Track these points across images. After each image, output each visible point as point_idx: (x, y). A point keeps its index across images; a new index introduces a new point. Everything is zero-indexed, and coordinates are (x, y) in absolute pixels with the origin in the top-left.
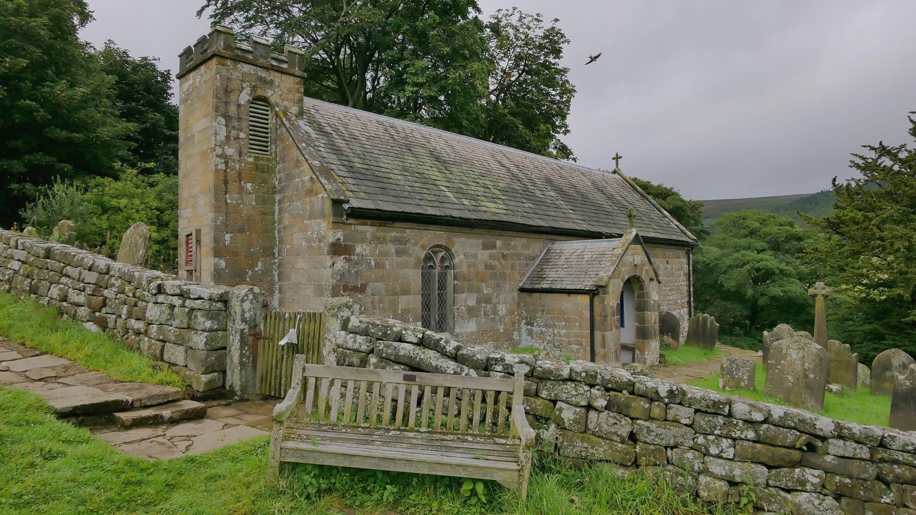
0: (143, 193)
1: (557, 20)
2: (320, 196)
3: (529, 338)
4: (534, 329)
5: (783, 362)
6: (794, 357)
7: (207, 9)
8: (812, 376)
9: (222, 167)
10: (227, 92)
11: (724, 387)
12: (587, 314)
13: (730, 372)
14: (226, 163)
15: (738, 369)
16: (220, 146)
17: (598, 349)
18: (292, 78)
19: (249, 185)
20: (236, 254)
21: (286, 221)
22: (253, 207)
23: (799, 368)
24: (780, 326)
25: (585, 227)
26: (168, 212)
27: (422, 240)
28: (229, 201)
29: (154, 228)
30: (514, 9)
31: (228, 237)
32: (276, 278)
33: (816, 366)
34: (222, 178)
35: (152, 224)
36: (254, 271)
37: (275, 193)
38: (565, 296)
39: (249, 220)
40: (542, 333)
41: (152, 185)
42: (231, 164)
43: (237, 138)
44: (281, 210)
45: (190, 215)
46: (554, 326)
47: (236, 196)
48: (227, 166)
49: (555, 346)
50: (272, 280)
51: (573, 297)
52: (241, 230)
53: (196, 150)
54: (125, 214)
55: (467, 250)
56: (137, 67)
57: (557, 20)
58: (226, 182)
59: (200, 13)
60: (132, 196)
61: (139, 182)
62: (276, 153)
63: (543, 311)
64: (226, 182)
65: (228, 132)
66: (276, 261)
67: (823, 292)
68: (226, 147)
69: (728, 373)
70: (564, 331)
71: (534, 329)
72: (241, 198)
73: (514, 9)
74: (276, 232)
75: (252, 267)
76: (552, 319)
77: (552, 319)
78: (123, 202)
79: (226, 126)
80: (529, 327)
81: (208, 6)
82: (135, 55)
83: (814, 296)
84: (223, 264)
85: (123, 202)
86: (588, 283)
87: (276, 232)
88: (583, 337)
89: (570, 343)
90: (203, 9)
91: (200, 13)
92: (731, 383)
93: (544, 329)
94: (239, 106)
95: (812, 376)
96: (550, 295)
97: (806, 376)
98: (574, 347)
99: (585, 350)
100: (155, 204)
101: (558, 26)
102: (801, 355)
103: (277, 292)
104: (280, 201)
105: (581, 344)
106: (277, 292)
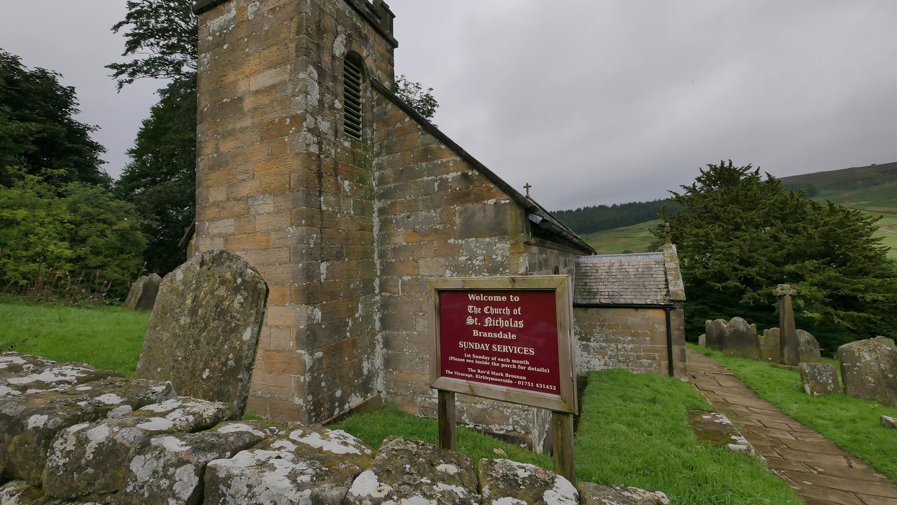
0: (50, 204)
1: (431, 89)
2: (491, 202)
3: (585, 354)
4: (590, 344)
5: (858, 364)
6: (868, 358)
7: (125, 26)
8: (891, 376)
9: (314, 149)
10: (320, 31)
11: (812, 393)
12: (663, 328)
13: (814, 378)
14: (319, 143)
15: (820, 374)
16: (312, 114)
17: (677, 363)
18: (384, 42)
19: (347, 183)
20: (333, 295)
21: (400, 238)
22: (351, 217)
23: (876, 369)
24: (735, 318)
26: (85, 226)
28: (324, 208)
29: (66, 244)
30: (402, 76)
31: (323, 267)
32: (378, 325)
33: (892, 366)
34: (314, 167)
35: (63, 239)
36: (355, 320)
37: (372, 198)
38: (632, 311)
39: (347, 239)
40: (601, 348)
41: (60, 195)
42: (325, 147)
43: (332, 107)
44: (384, 224)
45: (232, 230)
46: (617, 341)
47: (332, 199)
48: (320, 149)
49: (619, 361)
50: (373, 329)
51: (640, 312)
52: (339, 256)
53: (248, 122)
54: (23, 228)
56: (29, 78)
57: (431, 89)
58: (320, 176)
59: (116, 27)
60: (33, 207)
61: (43, 191)
62: (372, 139)
63: (602, 326)
64: (320, 176)
65: (322, 94)
66: (377, 298)
67: (790, 292)
68: (319, 119)
69: (812, 379)
70: (631, 346)
71: (590, 344)
72: (338, 204)
73: (402, 76)
74: (376, 256)
75: (352, 312)
76: (614, 334)
77: (614, 334)
78: (21, 214)
79: (319, 83)
80: (584, 342)
81: (128, 23)
82: (29, 65)
83: (781, 297)
84: (318, 314)
85: (21, 214)
86: (660, 298)
87: (376, 256)
88: (655, 350)
89: (639, 357)
90: (120, 24)
91: (116, 27)
92: (817, 388)
93: (604, 344)
94: (334, 57)
95: (891, 376)
96: (611, 311)
97: (886, 377)
98: (645, 361)
99: (659, 365)
100: (68, 217)
101: (431, 94)
102: (874, 356)
103: (379, 347)
104: (382, 211)
105: (654, 358)
106: (379, 347)
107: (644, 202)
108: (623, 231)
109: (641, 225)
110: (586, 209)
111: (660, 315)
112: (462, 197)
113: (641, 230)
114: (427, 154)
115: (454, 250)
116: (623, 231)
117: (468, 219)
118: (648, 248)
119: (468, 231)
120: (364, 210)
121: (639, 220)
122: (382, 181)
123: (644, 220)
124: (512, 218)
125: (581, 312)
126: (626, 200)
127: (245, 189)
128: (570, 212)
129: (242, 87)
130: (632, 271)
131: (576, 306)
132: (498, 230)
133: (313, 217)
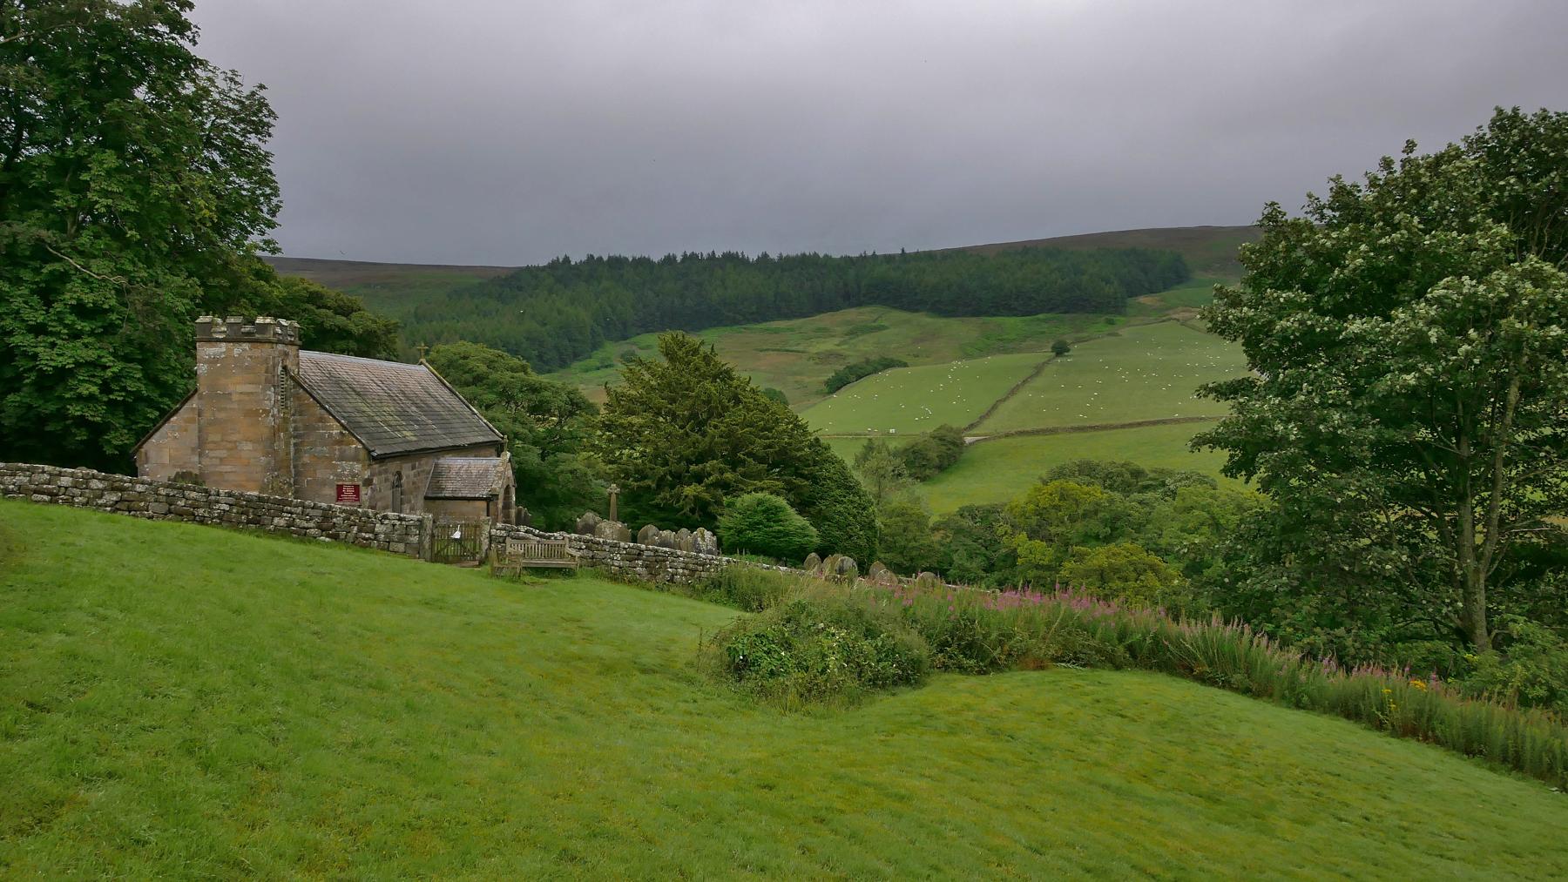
1: (262, 87)
21: (306, 459)
25: (449, 442)
27: (393, 466)
44: (297, 451)
55: (408, 472)
57: (262, 87)
86: (484, 493)
107: (836, 255)
108: (776, 331)
109: (823, 320)
110: (691, 259)
111: (484, 504)
112: (340, 443)
113: (824, 332)
114: (321, 419)
115: (335, 467)
116: (776, 331)
117: (342, 452)
118: (827, 383)
119: (341, 459)
120: (287, 444)
121: (821, 305)
122: (295, 429)
123: (833, 308)
124: (363, 454)
125: (430, 503)
126: (794, 249)
127: (234, 438)
128: (643, 262)
129: (231, 388)
130: (474, 472)
131: (426, 498)
132: (356, 459)
133: (271, 452)
